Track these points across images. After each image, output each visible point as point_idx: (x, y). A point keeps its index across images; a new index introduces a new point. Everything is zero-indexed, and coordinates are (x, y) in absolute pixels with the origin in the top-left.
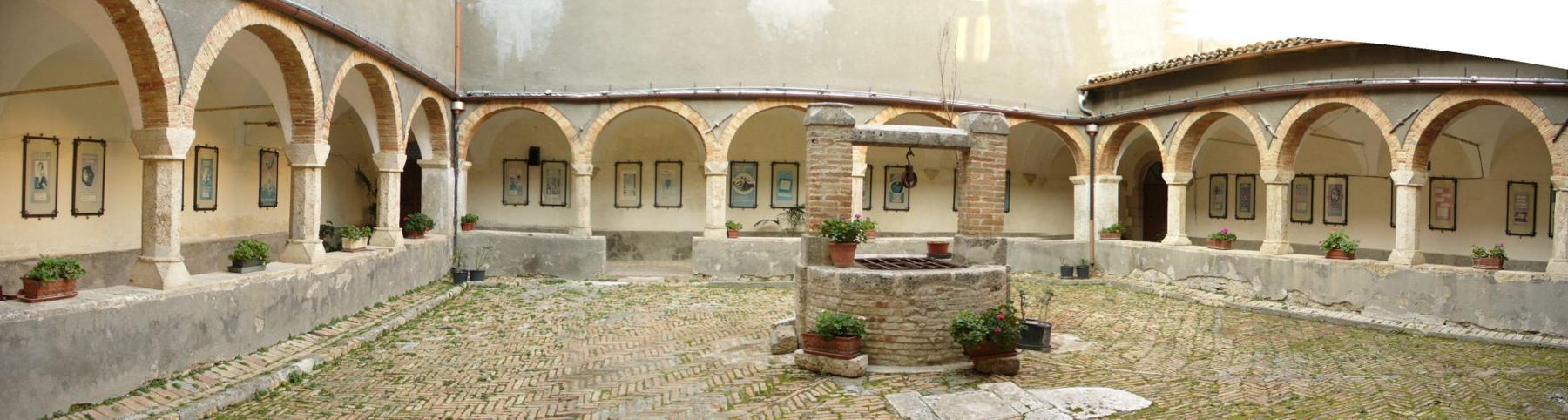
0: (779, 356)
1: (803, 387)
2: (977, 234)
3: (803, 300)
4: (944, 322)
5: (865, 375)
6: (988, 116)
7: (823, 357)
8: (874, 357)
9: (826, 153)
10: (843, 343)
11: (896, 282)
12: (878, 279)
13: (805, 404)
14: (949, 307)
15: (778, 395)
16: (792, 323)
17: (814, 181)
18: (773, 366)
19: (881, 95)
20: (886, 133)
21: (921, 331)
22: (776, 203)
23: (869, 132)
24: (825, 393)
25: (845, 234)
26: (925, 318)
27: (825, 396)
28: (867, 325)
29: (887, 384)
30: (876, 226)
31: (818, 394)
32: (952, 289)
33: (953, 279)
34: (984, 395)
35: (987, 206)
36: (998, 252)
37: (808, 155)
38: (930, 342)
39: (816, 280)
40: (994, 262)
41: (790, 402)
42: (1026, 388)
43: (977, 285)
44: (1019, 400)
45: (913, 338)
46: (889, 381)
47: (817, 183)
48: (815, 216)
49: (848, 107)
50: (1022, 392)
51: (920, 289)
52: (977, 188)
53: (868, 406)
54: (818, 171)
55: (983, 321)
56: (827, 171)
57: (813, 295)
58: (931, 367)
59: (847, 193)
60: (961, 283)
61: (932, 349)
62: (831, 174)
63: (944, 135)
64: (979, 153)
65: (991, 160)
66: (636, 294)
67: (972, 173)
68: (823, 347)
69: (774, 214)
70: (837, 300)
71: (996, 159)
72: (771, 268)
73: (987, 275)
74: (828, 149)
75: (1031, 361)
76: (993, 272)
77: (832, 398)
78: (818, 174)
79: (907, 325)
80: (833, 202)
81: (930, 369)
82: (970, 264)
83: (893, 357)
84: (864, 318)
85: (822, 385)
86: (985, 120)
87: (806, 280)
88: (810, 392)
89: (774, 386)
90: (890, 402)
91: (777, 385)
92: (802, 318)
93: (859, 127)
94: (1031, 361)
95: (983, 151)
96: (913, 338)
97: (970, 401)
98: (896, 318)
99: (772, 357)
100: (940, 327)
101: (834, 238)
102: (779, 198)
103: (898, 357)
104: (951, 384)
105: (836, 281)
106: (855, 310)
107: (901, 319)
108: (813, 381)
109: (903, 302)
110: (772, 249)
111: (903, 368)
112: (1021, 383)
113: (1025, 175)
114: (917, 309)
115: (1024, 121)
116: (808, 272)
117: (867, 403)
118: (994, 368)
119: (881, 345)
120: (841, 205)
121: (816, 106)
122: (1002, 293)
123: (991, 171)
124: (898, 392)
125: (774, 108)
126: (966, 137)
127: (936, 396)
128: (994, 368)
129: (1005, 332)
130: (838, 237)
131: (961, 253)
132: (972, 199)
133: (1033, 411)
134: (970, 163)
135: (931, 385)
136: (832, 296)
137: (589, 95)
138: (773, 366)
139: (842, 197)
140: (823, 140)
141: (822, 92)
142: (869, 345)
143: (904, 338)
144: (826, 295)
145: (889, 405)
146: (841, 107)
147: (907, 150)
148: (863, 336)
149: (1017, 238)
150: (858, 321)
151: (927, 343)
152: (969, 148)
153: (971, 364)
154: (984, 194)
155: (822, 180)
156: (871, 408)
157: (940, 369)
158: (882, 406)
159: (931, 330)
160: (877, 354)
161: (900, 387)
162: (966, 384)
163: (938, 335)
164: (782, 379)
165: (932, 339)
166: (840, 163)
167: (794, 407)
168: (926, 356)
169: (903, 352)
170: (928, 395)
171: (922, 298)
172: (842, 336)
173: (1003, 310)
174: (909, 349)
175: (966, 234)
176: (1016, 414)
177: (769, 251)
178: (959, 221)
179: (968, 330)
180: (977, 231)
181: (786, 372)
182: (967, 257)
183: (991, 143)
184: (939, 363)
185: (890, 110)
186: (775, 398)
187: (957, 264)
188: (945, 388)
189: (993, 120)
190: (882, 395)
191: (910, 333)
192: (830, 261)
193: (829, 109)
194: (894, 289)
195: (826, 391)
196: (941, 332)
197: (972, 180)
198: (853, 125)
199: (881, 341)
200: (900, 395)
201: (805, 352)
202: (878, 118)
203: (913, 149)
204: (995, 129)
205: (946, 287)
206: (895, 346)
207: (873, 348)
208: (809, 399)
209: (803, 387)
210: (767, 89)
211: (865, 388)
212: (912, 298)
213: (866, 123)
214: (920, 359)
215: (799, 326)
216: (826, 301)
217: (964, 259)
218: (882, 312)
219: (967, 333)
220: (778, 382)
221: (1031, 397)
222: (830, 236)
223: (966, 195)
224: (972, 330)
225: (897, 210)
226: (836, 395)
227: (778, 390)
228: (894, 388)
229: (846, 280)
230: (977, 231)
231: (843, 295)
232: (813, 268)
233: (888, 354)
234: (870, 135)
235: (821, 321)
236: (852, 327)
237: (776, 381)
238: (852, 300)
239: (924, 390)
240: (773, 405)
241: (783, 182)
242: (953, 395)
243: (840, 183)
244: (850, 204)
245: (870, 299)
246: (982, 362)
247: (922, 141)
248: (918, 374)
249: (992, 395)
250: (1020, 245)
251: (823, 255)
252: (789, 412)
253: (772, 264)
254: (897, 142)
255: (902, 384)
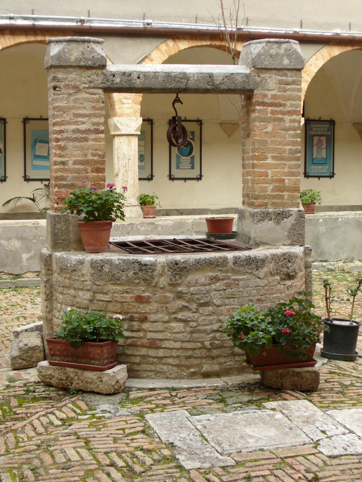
0: (22, 372)
1: (47, 408)
2: (266, 205)
3: (49, 298)
4: (220, 321)
5: (123, 391)
6: (275, 46)
7: (72, 370)
8: (136, 367)
9: (72, 104)
10: (95, 350)
11: (159, 268)
12: (137, 266)
13: (46, 429)
14: (227, 301)
15: (16, 419)
16: (39, 328)
17: (57, 140)
18: (12, 384)
19: (157, 24)
20: (168, 75)
21: (192, 332)
22: (31, 174)
23: (124, 74)
24: (72, 415)
25: (97, 209)
26: (196, 315)
27: (72, 419)
28: (126, 326)
29: (150, 402)
30: (156, 201)
31: (63, 416)
32: (229, 278)
33: (231, 264)
34: (269, 415)
35: (276, 166)
36: (293, 228)
37: (50, 106)
38: (204, 347)
39: (63, 270)
40: (289, 242)
41: (28, 428)
42: (325, 408)
43: (262, 272)
44: (314, 423)
45: (183, 342)
46: (153, 398)
47: (62, 143)
48: (60, 187)
49: (98, 43)
50: (319, 413)
51: (189, 279)
52: (264, 143)
53: (123, 429)
54: (62, 128)
55: (269, 319)
56: (73, 127)
57: (60, 289)
58: (206, 380)
59: (99, 156)
60: (242, 269)
61: (207, 357)
62: (78, 131)
63: (219, 74)
64: (265, 96)
65: (280, 105)
66: (64, 378)
67: (257, 124)
68: (72, 356)
69: (30, 189)
70: (88, 295)
71: (288, 103)
72: (24, 260)
73: (275, 258)
74: (72, 98)
75: (338, 374)
76: (284, 254)
77: (80, 421)
78: (61, 132)
79: (174, 324)
80: (82, 167)
81: (205, 383)
82: (257, 245)
83: (159, 367)
84: (121, 317)
85: (70, 405)
86: (273, 52)
87: (52, 270)
88: (54, 414)
89: (11, 409)
90: (151, 423)
91: (16, 407)
92: (49, 321)
93: (111, 67)
94: (338, 374)
95: (270, 94)
96: (183, 342)
97: (249, 423)
98: (159, 316)
99: (12, 373)
100: (216, 327)
101: (83, 215)
102: (36, 167)
103: (165, 367)
104: (229, 401)
105: (86, 270)
106: (111, 307)
107: (167, 318)
108: (60, 400)
109: (167, 294)
110: (24, 235)
111: (172, 381)
112: (320, 402)
113: (355, 124)
114: (187, 304)
115: (349, 48)
116: (54, 261)
117: (122, 425)
118: (287, 382)
119: (144, 351)
120: (92, 172)
121: (57, 42)
122: (298, 283)
123: (282, 120)
124: (162, 411)
125: (21, 44)
126: (247, 76)
127: (208, 416)
128: (287, 382)
129: (296, 333)
130: (87, 213)
131: (246, 230)
132: (258, 159)
133: (329, 437)
134: (254, 111)
135: (204, 402)
136: (82, 290)
137: (20, 22)
138: (12, 384)
139: (93, 161)
140: (67, 86)
141: (82, 21)
142: (129, 352)
143: (172, 342)
144: (75, 289)
145: (149, 427)
146: (89, 42)
147: (174, 96)
148: (121, 341)
149: (342, 213)
150: (114, 321)
151: (200, 348)
152: (252, 91)
153: (258, 376)
154: (274, 150)
155: (69, 139)
156: (127, 431)
157: (218, 382)
158: (140, 429)
159: (205, 331)
160: (139, 364)
161: (165, 405)
162: (249, 401)
163: (214, 338)
164: (22, 399)
165: (207, 344)
166: (89, 116)
167: (32, 434)
168: (200, 365)
169: (171, 361)
170: (199, 415)
171: (192, 289)
172: (95, 340)
173: (296, 306)
174: (178, 357)
175: (251, 205)
176: (307, 440)
177: (21, 238)
178: (243, 190)
179: (247, 330)
180: (266, 201)
181: (28, 391)
182: (253, 235)
183: (281, 82)
184: (217, 375)
185: (170, 43)
186: (9, 424)
187: (241, 245)
188: (221, 405)
189: (282, 51)
190: (141, 415)
191: (179, 336)
192: (81, 247)
193: (73, 45)
194: (156, 279)
195: (75, 412)
196: (218, 334)
197: (257, 132)
198: (104, 67)
199: (143, 346)
200: (163, 414)
201: (51, 364)
202: (155, 55)
203: (180, 96)
204: (286, 62)
205: (220, 275)
206: (161, 353)
207: (134, 356)
208: (51, 423)
209: (47, 408)
210: (11, 18)
211: (123, 407)
212: (180, 289)
213: (140, 63)
214: (192, 370)
215: (46, 332)
216: (75, 297)
217: (250, 238)
218: (144, 308)
219: (247, 334)
220: (16, 404)
221: (330, 420)
222: (79, 212)
223: (251, 154)
224: (253, 330)
225: (185, 179)
226: (86, 417)
227: (15, 413)
228: (157, 406)
229: (98, 267)
230: (266, 201)
231: (95, 287)
232: (58, 254)
233: (153, 363)
234: (125, 78)
235: (67, 322)
236: (107, 329)
237: (14, 402)
238: (106, 293)
239: (194, 408)
240: (7, 432)
241: (38, 144)
242: (230, 414)
243: (90, 143)
244: (102, 170)
245: (127, 292)
246: (270, 373)
247: (191, 84)
248: (189, 389)
249: (279, 416)
250: (347, 222)
251: (72, 237)
252: (26, 439)
253: (25, 256)
254: (158, 86)
255: (167, 402)
